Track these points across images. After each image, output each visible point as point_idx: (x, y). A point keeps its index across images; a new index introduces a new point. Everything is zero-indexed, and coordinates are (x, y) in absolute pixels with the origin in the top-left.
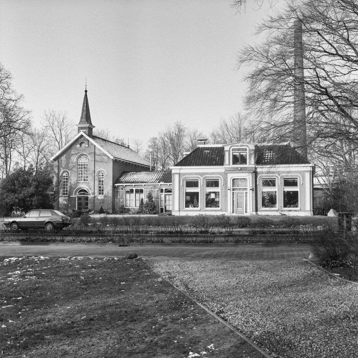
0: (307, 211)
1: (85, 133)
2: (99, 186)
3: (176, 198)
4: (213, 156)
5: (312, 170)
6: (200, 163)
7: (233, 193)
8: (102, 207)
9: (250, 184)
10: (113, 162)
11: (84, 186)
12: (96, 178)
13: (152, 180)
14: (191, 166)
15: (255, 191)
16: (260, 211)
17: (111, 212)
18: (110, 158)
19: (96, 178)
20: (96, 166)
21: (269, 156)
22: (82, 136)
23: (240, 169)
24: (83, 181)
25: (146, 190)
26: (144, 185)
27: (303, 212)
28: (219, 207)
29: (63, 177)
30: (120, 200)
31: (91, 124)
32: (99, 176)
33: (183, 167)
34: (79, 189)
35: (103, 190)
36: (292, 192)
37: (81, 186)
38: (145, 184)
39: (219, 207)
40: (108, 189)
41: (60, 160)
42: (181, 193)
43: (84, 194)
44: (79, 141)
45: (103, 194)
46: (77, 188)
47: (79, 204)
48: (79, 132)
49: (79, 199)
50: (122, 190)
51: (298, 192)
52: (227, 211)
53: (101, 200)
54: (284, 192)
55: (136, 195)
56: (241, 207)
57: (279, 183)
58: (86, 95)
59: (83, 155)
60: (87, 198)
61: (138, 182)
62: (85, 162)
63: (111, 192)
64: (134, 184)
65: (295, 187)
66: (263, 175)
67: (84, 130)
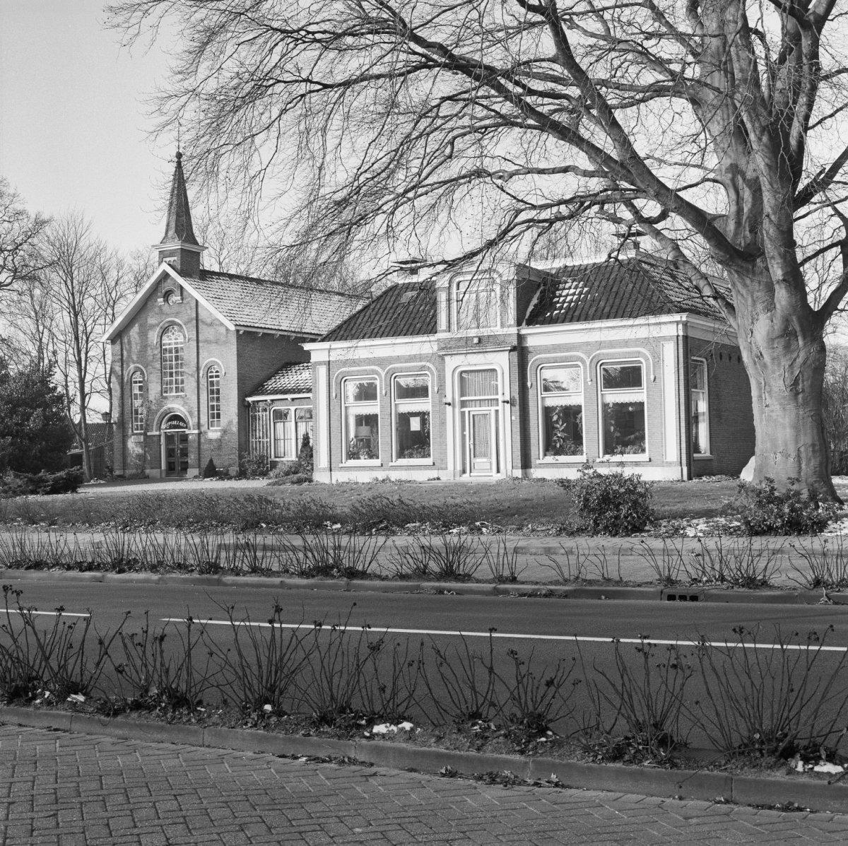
0: (670, 464)
2: (210, 404)
3: (321, 430)
5: (681, 333)
7: (463, 414)
8: (211, 461)
9: (505, 387)
11: (177, 407)
12: (203, 382)
14: (608, 317)
15: (518, 407)
16: (536, 467)
17: (234, 470)
19: (203, 382)
20: (201, 351)
21: (569, 298)
22: (165, 276)
23: (476, 340)
27: (659, 469)
28: (643, 451)
30: (261, 440)
32: (211, 377)
34: (170, 410)
36: (631, 404)
37: (170, 406)
41: (126, 340)
42: (334, 417)
43: (178, 427)
44: (161, 289)
47: (170, 453)
48: (160, 263)
49: (169, 438)
51: (377, 415)
52: (446, 468)
53: (216, 440)
54: (605, 406)
55: (299, 424)
56: (485, 455)
57: (589, 379)
59: (173, 323)
60: (184, 438)
61: (300, 391)
62: (176, 343)
63: (235, 420)
64: (289, 396)
65: (636, 389)
66: (603, 351)
67: (172, 259)
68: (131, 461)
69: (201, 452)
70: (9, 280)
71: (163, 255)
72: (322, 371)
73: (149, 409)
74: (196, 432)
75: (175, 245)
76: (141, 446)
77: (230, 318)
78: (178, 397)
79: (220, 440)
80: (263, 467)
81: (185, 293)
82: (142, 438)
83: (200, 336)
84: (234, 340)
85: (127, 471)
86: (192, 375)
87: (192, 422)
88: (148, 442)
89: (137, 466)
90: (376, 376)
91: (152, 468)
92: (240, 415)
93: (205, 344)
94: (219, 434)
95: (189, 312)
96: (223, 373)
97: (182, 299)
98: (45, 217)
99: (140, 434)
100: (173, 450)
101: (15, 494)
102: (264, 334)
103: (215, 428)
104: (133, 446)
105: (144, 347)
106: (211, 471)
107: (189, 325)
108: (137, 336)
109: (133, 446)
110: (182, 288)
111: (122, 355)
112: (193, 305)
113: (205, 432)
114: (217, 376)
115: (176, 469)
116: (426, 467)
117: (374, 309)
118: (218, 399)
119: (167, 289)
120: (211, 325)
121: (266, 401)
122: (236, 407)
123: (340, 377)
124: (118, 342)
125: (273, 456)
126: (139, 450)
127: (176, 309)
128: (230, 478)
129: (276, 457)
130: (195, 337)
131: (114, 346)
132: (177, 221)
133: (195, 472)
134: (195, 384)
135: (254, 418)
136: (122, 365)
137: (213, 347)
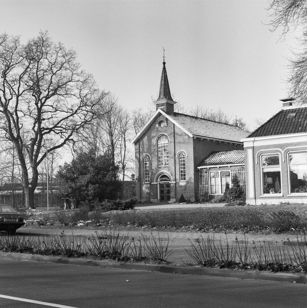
1: (163, 111)
2: (180, 170)
4: (299, 120)
6: (280, 131)
8: (182, 195)
10: (193, 141)
11: (166, 172)
12: (177, 160)
13: (241, 160)
18: (190, 137)
20: (176, 147)
22: (160, 114)
24: (163, 166)
25: (232, 172)
26: (231, 166)
29: (145, 162)
30: (205, 186)
31: (172, 100)
32: (181, 158)
33: (257, 139)
34: (162, 173)
35: (185, 175)
37: (162, 171)
38: (231, 165)
39: (280, 192)
40: (190, 173)
43: (167, 180)
44: (158, 120)
45: (185, 179)
46: (158, 173)
47: (162, 192)
48: (157, 109)
49: (161, 186)
50: (206, 174)
53: (184, 186)
55: (222, 178)
58: (164, 68)
59: (163, 135)
60: (168, 185)
61: (223, 164)
63: (193, 177)
64: (218, 166)
67: (162, 107)
68: (144, 195)
69: (177, 191)
70: (90, 119)
71: (158, 106)
72: (250, 152)
73: (152, 173)
74: (174, 182)
75: (164, 101)
76: (149, 189)
77: (190, 132)
78: (166, 167)
79: (185, 186)
80: (208, 198)
81: (169, 122)
82: (149, 185)
83: (176, 140)
84: (192, 142)
85: (142, 200)
86: (172, 158)
87: (172, 178)
88: (152, 187)
89: (147, 198)
90: (278, 153)
91: (154, 199)
92: (195, 175)
93: (178, 144)
94: (185, 183)
95: (171, 130)
96: (187, 156)
97: (167, 124)
98: (106, 92)
99: (148, 184)
100: (163, 190)
101: (108, 210)
102: (204, 139)
103: (183, 181)
104: (145, 189)
105: (150, 145)
106: (182, 200)
107: (171, 136)
108: (146, 141)
109: (145, 189)
110: (167, 119)
111: (140, 150)
112: (172, 127)
113: (179, 183)
114: (184, 158)
115: (165, 199)
116: (279, 198)
117: (273, 122)
118: (184, 168)
119: (160, 120)
120: (181, 135)
121: (207, 168)
122: (193, 171)
123: (260, 154)
124: (138, 144)
125: (210, 193)
126: (147, 191)
127: (165, 129)
128: (192, 203)
129: (211, 193)
130: (173, 141)
131: (136, 146)
132: (164, 91)
133: (174, 200)
134: (174, 162)
135: (201, 176)
136: (140, 154)
137: (181, 145)
